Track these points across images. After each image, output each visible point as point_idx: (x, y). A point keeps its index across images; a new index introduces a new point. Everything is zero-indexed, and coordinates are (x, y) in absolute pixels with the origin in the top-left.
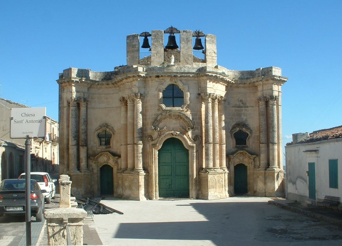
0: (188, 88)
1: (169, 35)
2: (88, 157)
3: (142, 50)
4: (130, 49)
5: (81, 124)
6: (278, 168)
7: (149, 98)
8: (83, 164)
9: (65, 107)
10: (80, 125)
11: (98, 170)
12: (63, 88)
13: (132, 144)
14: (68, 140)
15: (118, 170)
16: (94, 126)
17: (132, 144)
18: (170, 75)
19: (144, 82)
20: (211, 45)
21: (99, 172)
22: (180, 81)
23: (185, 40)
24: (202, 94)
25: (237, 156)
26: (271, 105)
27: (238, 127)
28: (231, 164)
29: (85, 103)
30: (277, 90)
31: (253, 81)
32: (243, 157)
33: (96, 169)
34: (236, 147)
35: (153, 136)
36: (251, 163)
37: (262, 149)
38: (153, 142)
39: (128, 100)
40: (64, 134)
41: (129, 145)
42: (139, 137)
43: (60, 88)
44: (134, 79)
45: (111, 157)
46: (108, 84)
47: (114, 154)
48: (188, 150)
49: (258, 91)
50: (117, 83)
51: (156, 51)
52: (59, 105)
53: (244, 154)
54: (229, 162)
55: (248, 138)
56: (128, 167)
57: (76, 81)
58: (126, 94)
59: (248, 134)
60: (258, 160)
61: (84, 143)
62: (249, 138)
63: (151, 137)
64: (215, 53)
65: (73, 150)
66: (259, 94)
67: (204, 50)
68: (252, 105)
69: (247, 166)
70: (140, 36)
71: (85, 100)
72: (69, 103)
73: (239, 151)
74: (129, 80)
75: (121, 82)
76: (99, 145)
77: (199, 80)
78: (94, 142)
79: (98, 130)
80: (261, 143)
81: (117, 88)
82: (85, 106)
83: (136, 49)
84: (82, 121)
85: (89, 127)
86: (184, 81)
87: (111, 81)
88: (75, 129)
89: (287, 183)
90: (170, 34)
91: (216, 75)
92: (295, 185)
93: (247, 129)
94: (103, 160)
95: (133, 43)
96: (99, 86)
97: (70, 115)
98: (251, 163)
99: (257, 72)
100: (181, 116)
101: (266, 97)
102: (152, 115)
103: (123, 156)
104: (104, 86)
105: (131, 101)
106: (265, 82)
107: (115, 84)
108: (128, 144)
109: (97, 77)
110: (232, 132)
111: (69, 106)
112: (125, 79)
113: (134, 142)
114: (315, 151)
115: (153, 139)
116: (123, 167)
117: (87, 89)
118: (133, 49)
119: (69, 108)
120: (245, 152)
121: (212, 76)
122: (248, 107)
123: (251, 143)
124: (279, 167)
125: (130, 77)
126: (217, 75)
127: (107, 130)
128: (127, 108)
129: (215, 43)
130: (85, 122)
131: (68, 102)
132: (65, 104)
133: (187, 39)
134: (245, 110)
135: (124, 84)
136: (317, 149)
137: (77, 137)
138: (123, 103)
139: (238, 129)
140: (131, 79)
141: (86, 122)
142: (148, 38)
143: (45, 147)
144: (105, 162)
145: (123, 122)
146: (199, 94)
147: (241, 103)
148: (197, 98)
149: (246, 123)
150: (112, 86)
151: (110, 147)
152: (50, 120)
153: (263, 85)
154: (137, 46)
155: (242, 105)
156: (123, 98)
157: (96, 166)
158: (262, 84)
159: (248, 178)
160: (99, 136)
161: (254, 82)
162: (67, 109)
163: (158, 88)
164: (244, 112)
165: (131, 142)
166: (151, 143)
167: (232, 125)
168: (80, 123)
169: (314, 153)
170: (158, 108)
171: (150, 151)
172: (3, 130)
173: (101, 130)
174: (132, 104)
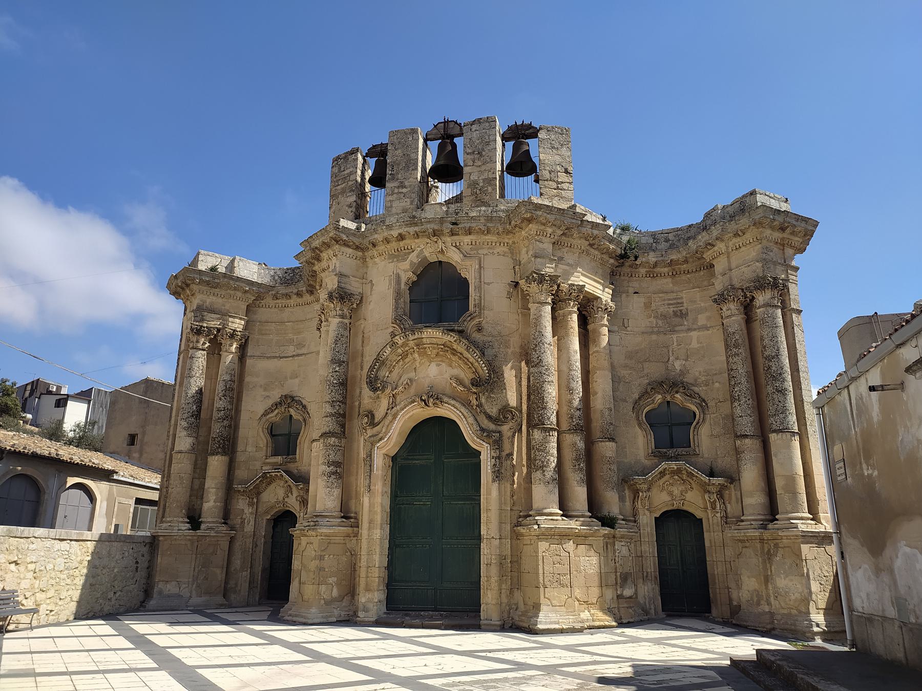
0: (477, 267)
2: (229, 490)
6: (813, 522)
7: (371, 307)
22: (454, 249)
27: (659, 393)
28: (640, 506)
32: (682, 488)
36: (714, 508)
42: (331, 415)
59: (694, 414)
63: (371, 415)
66: (719, 284)
69: (701, 520)
77: (514, 243)
93: (691, 396)
98: (714, 508)
106: (734, 240)
115: (376, 420)
123: (707, 439)
124: (816, 518)
130: (228, 389)
144: (278, 502)
146: (517, 284)
153: (729, 253)
157: (251, 513)
158: (724, 249)
160: (272, 431)
166: (370, 432)
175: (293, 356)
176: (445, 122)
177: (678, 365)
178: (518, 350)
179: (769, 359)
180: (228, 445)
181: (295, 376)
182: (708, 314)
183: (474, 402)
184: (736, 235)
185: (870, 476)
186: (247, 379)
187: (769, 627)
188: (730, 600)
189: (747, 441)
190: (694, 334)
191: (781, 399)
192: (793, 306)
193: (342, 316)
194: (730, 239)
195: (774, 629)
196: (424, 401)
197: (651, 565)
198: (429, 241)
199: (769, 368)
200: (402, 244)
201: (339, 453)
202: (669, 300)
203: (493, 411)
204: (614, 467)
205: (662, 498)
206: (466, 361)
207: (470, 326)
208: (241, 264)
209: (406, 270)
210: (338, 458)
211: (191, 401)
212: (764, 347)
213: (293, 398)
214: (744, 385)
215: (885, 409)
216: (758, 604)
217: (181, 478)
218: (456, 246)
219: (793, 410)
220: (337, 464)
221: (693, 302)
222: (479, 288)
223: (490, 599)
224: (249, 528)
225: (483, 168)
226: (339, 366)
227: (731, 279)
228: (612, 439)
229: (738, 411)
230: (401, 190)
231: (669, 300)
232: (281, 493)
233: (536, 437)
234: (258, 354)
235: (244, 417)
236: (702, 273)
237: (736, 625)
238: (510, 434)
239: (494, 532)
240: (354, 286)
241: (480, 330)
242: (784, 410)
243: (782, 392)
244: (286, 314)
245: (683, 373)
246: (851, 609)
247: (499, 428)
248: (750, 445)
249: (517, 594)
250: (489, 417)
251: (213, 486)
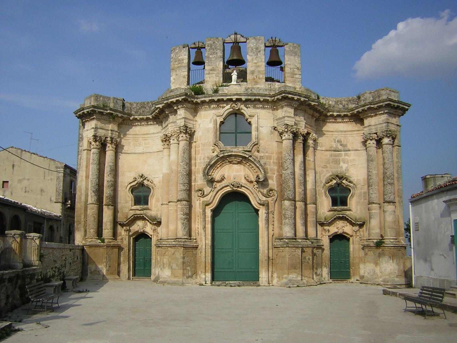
2: (115, 223)
8: (107, 232)
14: (87, 196)
16: (126, 178)
20: (293, 58)
23: (254, 49)
37: (372, 211)
38: (205, 199)
48: (257, 211)
51: (212, 67)
61: (110, 201)
64: (298, 69)
66: (366, 131)
68: (355, 148)
85: (120, 179)
88: (97, 180)
91: (299, 97)
94: (138, 226)
95: (179, 58)
97: (91, 161)
102: (204, 159)
109: (133, 110)
115: (205, 194)
121: (293, 99)
126: (300, 98)
129: (298, 55)
133: (257, 49)
134: (346, 155)
147: (339, 145)
148: (272, 133)
149: (347, 174)
155: (340, 147)
163: (213, 118)
164: (343, 157)
167: (325, 177)
168: (419, 198)
172: (26, 192)
212: (385, 163)
230: (213, 72)
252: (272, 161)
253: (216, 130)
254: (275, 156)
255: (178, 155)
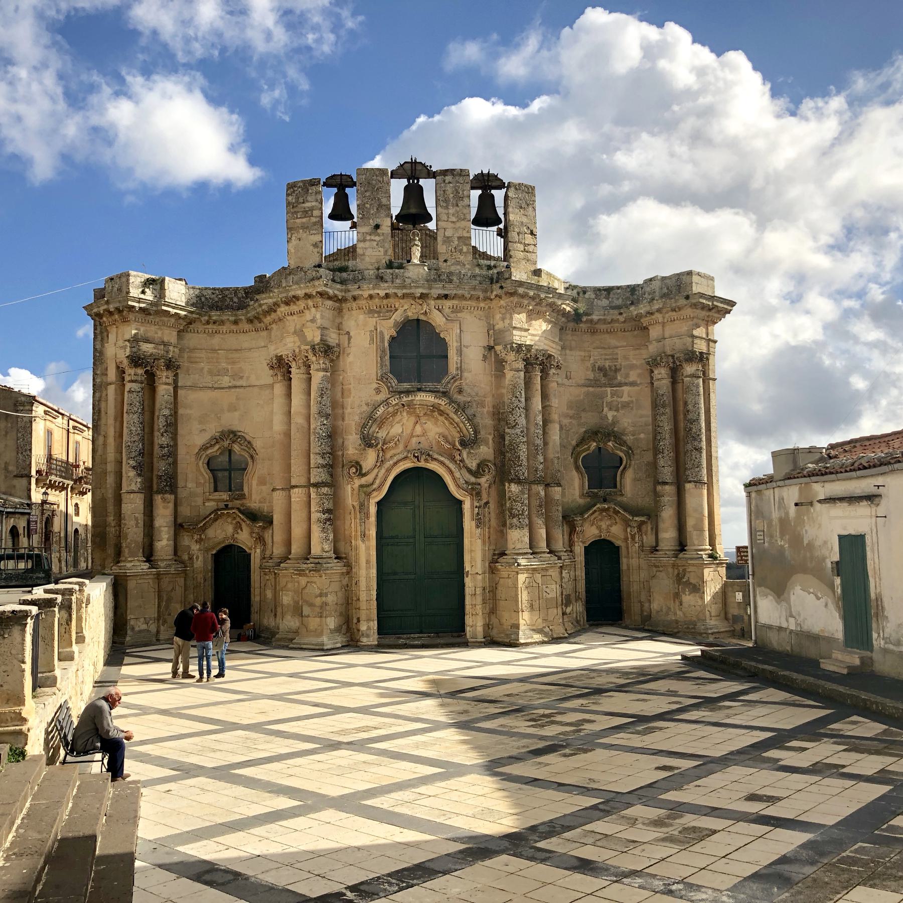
0: (458, 331)
1: (404, 182)
2: (179, 527)
3: (330, 225)
4: (298, 221)
5: (159, 430)
7: (350, 359)
9: (110, 384)
10: (156, 434)
11: (205, 562)
12: (107, 330)
13: (305, 486)
14: (119, 475)
15: (264, 558)
16: (194, 436)
17: (305, 486)
18: (408, 291)
19: (336, 313)
21: (210, 566)
22: (437, 312)
24: (498, 348)
25: (592, 517)
26: (687, 376)
27: (594, 441)
29: (170, 374)
30: (704, 336)
31: (636, 313)
32: (608, 523)
33: (201, 558)
34: (588, 495)
35: (361, 463)
38: (364, 480)
39: (293, 365)
40: (109, 460)
41: (296, 490)
42: (323, 466)
43: (98, 332)
44: (310, 303)
45: (243, 525)
46: (236, 322)
47: (253, 516)
49: (649, 341)
50: (261, 316)
52: (94, 379)
53: (611, 513)
54: (570, 535)
55: (622, 468)
56: (293, 551)
57: (140, 308)
58: (287, 346)
59: (621, 459)
60: (652, 529)
62: (625, 468)
63: (358, 465)
65: (133, 505)
66: (653, 348)
67: (501, 226)
69: (618, 547)
70: (325, 184)
71: (170, 365)
72: (124, 373)
73: (598, 506)
74: (294, 308)
75: (273, 315)
76: (212, 490)
77: (489, 308)
78: (194, 478)
79: (207, 448)
80: (659, 483)
81: (264, 333)
82: (170, 381)
83: (314, 220)
84: (160, 423)
86: (447, 311)
87: (244, 311)
89: (755, 597)
90: (409, 181)
92: (784, 604)
94: (222, 532)
96: (210, 326)
99: (648, 289)
100: (442, 408)
101: (673, 356)
103: (277, 518)
104: (224, 328)
105: (301, 365)
106: (670, 313)
107: (256, 321)
108: (296, 487)
110: (579, 454)
111: (123, 379)
112: (282, 305)
113: (309, 479)
114: (871, 498)
115: (364, 471)
116: (278, 551)
117: (175, 333)
118: (304, 220)
119: (124, 385)
120: (614, 509)
122: (620, 385)
123: (631, 484)
125: (296, 298)
127: (236, 448)
128: (289, 387)
130: (168, 425)
131: (118, 367)
132: (112, 375)
135: (280, 320)
136: (875, 491)
137: (144, 467)
138: (279, 374)
139: (595, 444)
140: (301, 304)
141: (172, 425)
142: (348, 190)
143: (74, 502)
145: (278, 425)
148: (485, 358)
150: (247, 326)
151: (242, 497)
152: (65, 418)
154: (316, 213)
156: (280, 359)
157: (200, 550)
159: (624, 578)
161: (639, 317)
162: (116, 390)
164: (609, 399)
165: (302, 481)
166: (358, 482)
168: (156, 427)
169: (865, 503)
170: (376, 386)
171: (353, 506)
173: (217, 447)
174: (305, 376)
175: (230, 387)
176: (412, 162)
177: (610, 415)
178: (491, 409)
179: (692, 422)
180: (171, 484)
181: (233, 408)
182: (639, 371)
183: (458, 458)
184: (673, 310)
185: (782, 546)
186: (181, 411)
187: (676, 630)
188: (642, 611)
189: (667, 487)
190: (626, 389)
191: (698, 456)
192: (711, 376)
193: (325, 370)
194: (667, 313)
195: (678, 632)
196: (417, 457)
197: (582, 586)
198: (413, 302)
199: (691, 429)
200: (385, 302)
201: (331, 501)
202: (606, 355)
203: (473, 464)
204: (560, 508)
205: (590, 532)
206: (452, 422)
207: (453, 388)
208: (170, 285)
209: (388, 329)
210: (331, 506)
211: (136, 438)
212: (688, 411)
213: (234, 433)
214: (667, 441)
215: (799, 515)
216: (667, 614)
217: (136, 519)
218: (438, 309)
219: (705, 465)
220: (329, 511)
221: (626, 358)
222: (460, 352)
223: (475, 623)
224: (199, 564)
225: (458, 225)
226: (327, 419)
227: (664, 345)
228: (559, 485)
229: (661, 462)
230: (373, 238)
231: (606, 355)
232: (230, 529)
233: (513, 489)
234: (189, 384)
235: (182, 451)
236: (636, 333)
237: (653, 629)
238: (487, 485)
239: (479, 568)
240: (333, 338)
241: (460, 391)
242: (699, 465)
243: (699, 450)
244: (216, 341)
245: (614, 423)
246: (756, 622)
247: (479, 480)
248: (669, 490)
249: (493, 617)
250: (470, 471)
251: (165, 524)
252: (485, 410)
253: (383, 351)
254: (489, 401)
255: (309, 394)
